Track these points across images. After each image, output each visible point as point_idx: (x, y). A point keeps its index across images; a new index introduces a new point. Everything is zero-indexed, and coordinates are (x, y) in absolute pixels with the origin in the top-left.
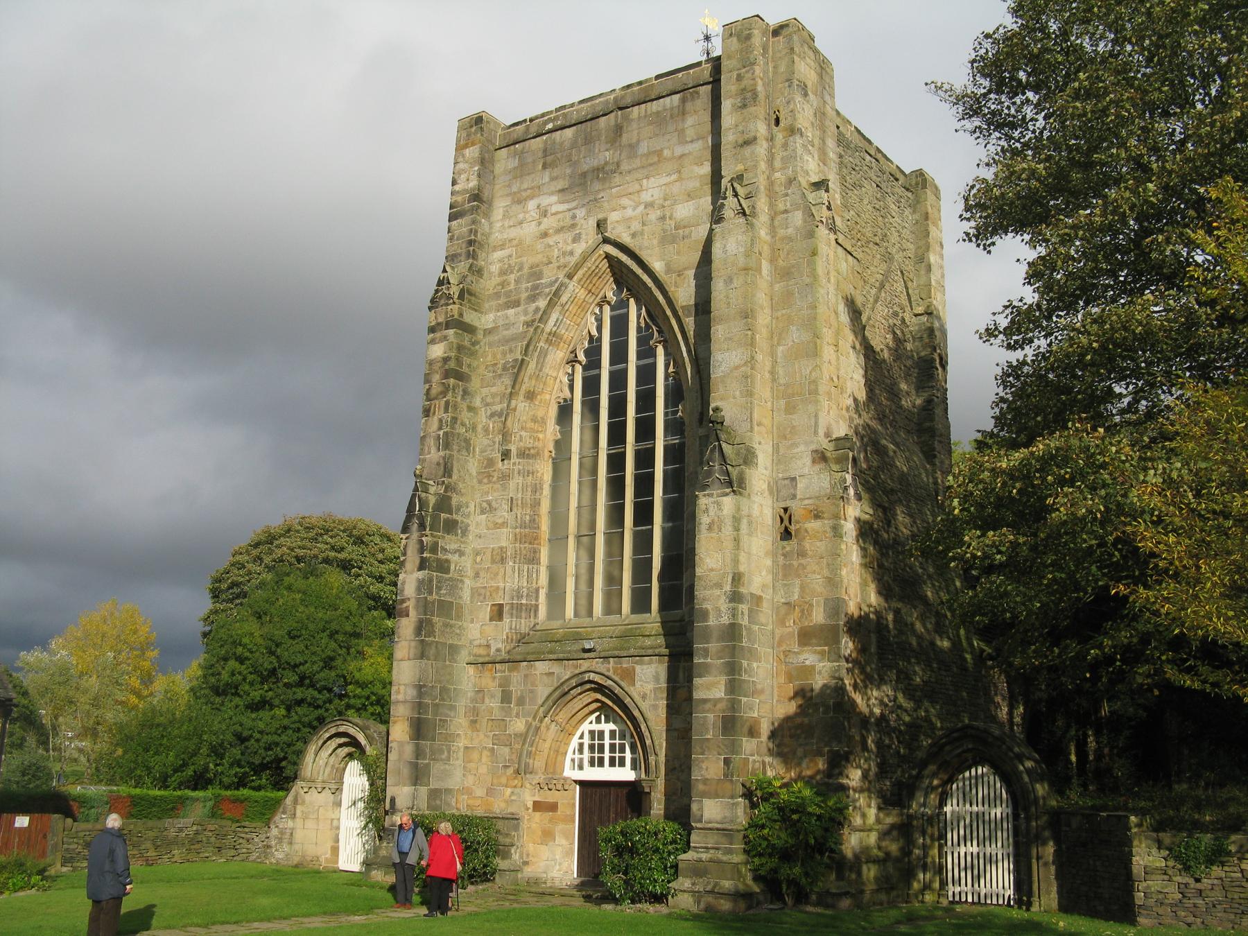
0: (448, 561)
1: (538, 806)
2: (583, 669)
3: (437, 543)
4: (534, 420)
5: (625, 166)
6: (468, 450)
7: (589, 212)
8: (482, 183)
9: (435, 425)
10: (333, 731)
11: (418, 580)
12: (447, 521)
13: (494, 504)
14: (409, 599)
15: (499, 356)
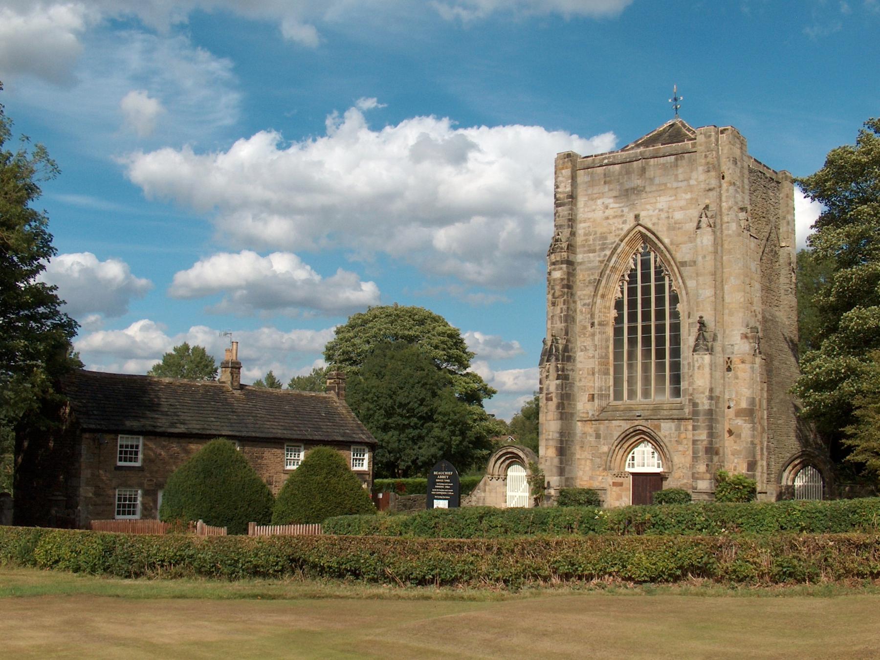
1: (614, 484)
4: (605, 308)
5: (648, 189)
6: (574, 321)
7: (631, 209)
9: (559, 311)
10: (504, 451)
12: (567, 356)
13: (587, 347)
15: (586, 276)
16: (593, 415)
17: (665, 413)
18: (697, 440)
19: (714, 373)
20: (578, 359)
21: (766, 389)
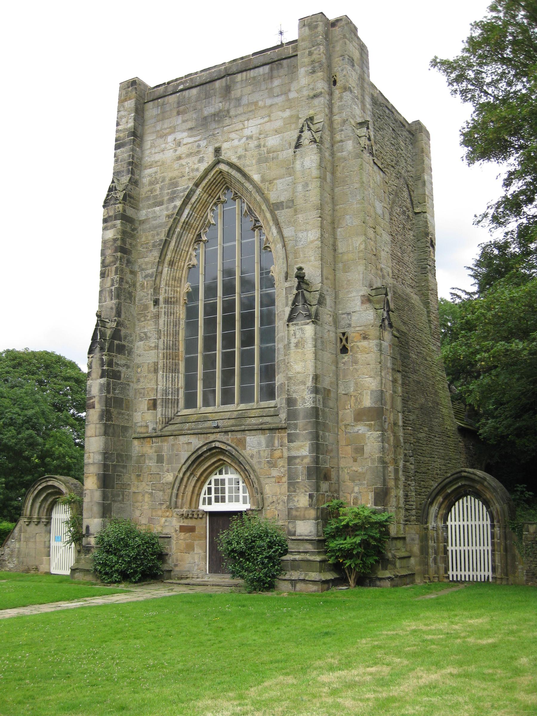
0: (119, 372)
2: (211, 440)
3: (112, 360)
5: (232, 113)
6: (130, 299)
8: (137, 124)
9: (109, 284)
10: (44, 485)
11: (101, 384)
12: (118, 345)
13: (149, 334)
14: (94, 397)
15: (150, 238)
16: (154, 429)
17: (253, 421)
18: (295, 457)
19: (320, 352)
20: (136, 351)
21: (400, 382)
